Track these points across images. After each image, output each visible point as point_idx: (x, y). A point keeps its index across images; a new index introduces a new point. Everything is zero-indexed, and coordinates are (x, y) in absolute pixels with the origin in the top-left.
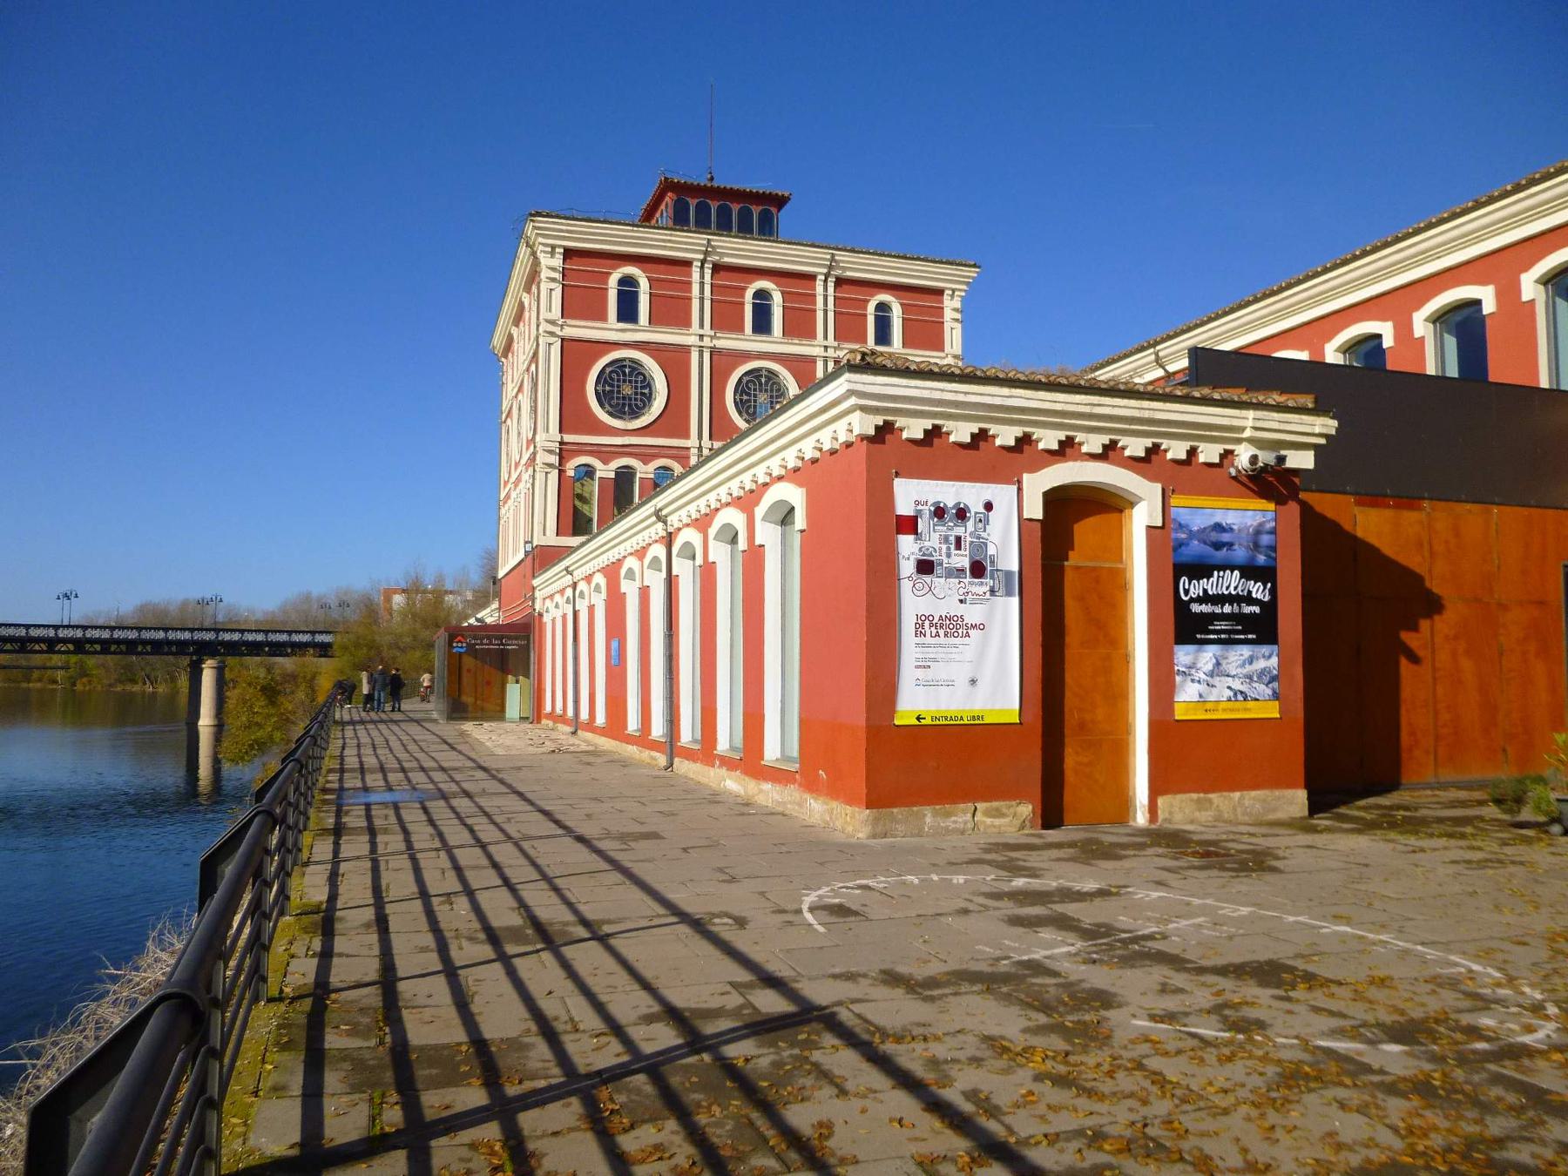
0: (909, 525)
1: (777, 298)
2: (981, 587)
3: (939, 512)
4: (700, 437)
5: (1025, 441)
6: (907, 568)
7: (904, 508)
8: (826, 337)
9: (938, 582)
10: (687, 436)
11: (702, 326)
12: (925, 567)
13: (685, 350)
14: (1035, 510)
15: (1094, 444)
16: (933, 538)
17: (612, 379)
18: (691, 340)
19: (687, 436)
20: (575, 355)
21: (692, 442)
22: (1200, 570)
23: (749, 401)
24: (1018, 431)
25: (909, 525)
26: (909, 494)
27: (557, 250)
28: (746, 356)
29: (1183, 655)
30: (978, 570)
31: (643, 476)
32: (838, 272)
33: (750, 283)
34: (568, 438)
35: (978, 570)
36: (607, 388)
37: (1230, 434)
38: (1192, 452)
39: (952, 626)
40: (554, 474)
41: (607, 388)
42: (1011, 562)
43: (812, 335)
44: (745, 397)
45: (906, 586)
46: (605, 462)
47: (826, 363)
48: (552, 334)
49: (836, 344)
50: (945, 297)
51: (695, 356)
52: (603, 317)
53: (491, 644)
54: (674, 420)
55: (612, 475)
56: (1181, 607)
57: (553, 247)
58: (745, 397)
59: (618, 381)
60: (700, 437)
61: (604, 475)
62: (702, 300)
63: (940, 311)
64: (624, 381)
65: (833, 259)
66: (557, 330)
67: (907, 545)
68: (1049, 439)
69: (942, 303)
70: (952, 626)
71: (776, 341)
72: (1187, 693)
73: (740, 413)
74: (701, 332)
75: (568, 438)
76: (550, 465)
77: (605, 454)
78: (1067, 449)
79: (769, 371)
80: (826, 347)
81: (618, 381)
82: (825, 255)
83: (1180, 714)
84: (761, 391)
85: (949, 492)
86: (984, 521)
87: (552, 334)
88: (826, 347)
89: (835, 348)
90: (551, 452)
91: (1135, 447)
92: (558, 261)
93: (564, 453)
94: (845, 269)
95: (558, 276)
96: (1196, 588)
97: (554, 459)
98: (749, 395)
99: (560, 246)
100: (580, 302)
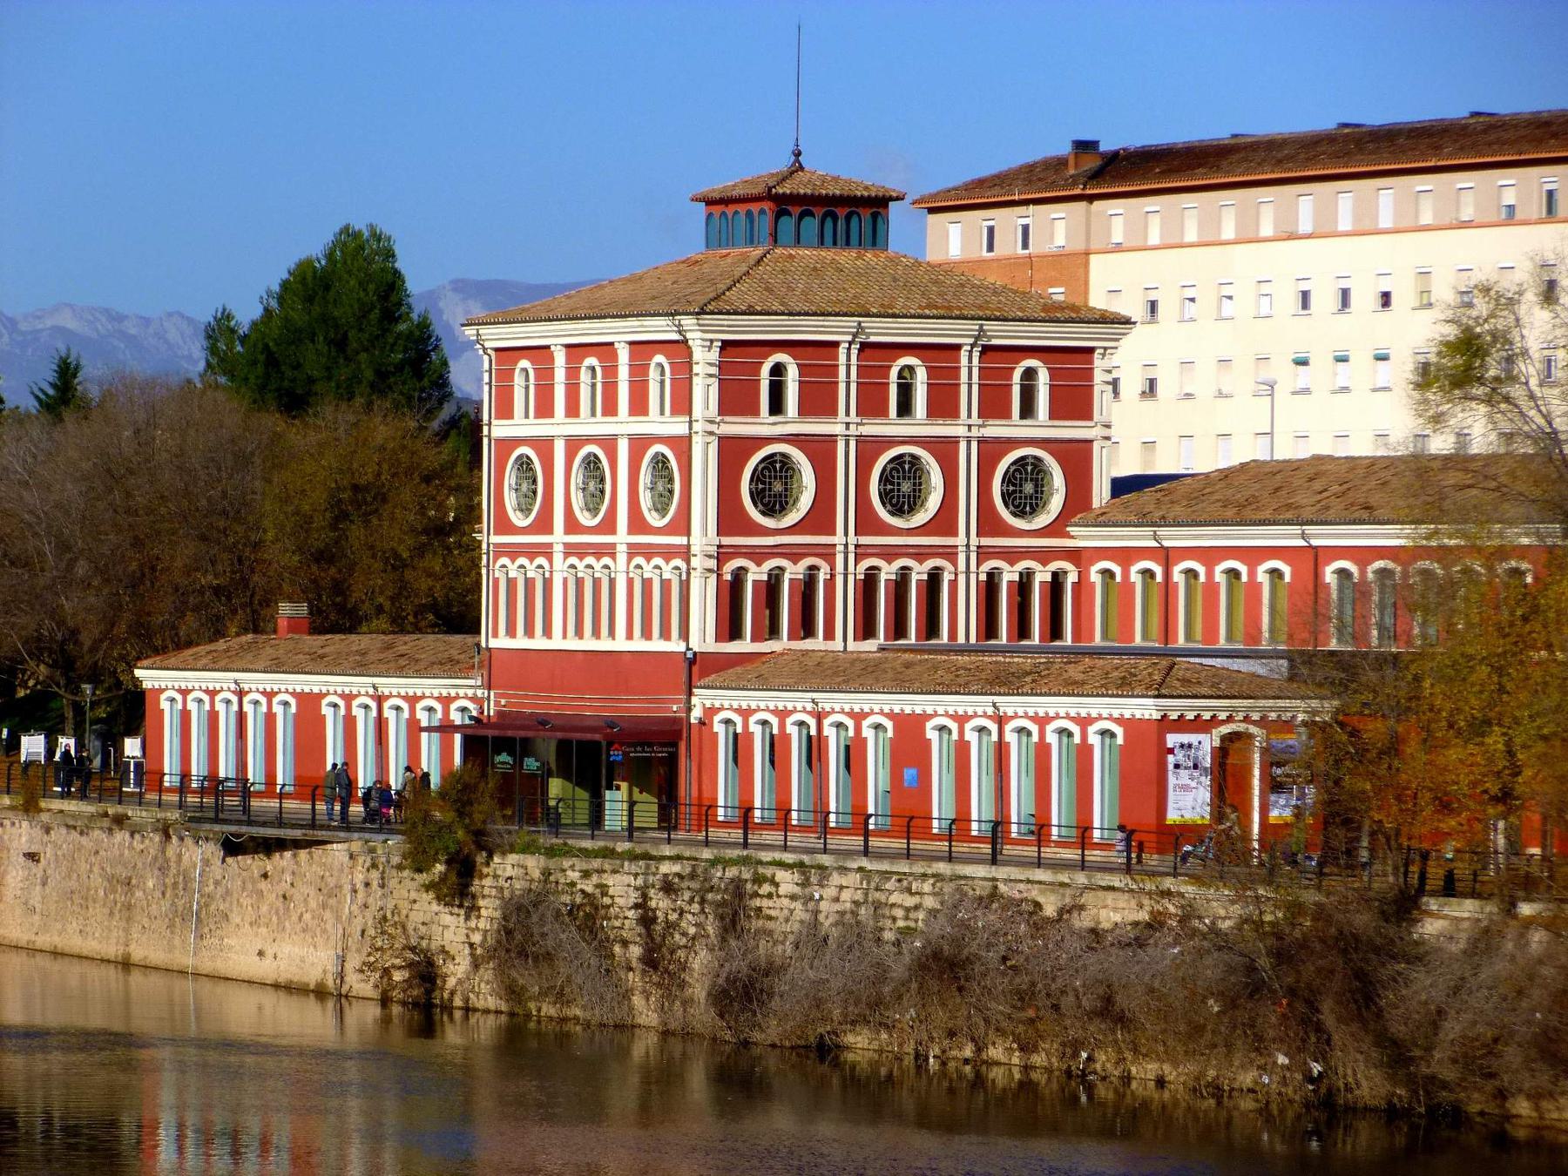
0: (1171, 751)
1: (921, 375)
2: (1196, 773)
3: (1182, 746)
4: (846, 534)
5: (1214, 717)
6: (1171, 767)
7: (1170, 745)
8: (969, 416)
9: (1182, 772)
10: (955, 533)
11: (848, 413)
12: (1177, 766)
13: (831, 439)
14: (1217, 743)
15: (1240, 716)
16: (1180, 756)
17: (764, 476)
18: (838, 429)
19: (833, 532)
20: (732, 451)
21: (960, 540)
22: (1279, 765)
23: (892, 490)
24: (1211, 713)
25: (1171, 751)
26: (1172, 740)
27: (715, 344)
28: (891, 442)
29: (1273, 798)
30: (1195, 767)
31: (793, 576)
32: (862, 338)
33: (766, 358)
34: (727, 541)
35: (1195, 767)
36: (760, 486)
37: (1296, 709)
38: (1279, 716)
39: (1185, 788)
40: (713, 578)
41: (760, 486)
42: (1207, 763)
43: (833, 412)
44: (889, 487)
45: (1170, 773)
46: (759, 564)
47: (969, 443)
48: (711, 433)
49: (980, 422)
50: (1096, 355)
51: (963, 446)
52: (755, 411)
53: (644, 751)
54: (821, 518)
55: (765, 578)
56: (1273, 779)
57: (712, 341)
58: (889, 487)
59: (770, 477)
60: (846, 534)
61: (758, 577)
62: (848, 384)
63: (1089, 374)
64: (775, 477)
65: (981, 329)
66: (713, 428)
67: (1171, 759)
68: (1223, 716)
69: (1092, 362)
70: (1185, 788)
71: (920, 424)
72: (1274, 814)
73: (884, 504)
74: (848, 420)
75: (727, 541)
76: (710, 570)
77: (1011, 556)
78: (1230, 719)
79: (913, 456)
80: (970, 426)
81: (770, 477)
82: (974, 326)
83: (1272, 821)
84: (904, 478)
85: (1185, 738)
86: (1197, 749)
87: (711, 433)
88: (970, 426)
89: (980, 426)
90: (710, 556)
91: (1256, 716)
92: (714, 355)
93: (722, 555)
94: (990, 338)
95: (714, 370)
96: (1279, 771)
97: (713, 564)
98: (893, 484)
99: (717, 340)
100: (735, 400)
